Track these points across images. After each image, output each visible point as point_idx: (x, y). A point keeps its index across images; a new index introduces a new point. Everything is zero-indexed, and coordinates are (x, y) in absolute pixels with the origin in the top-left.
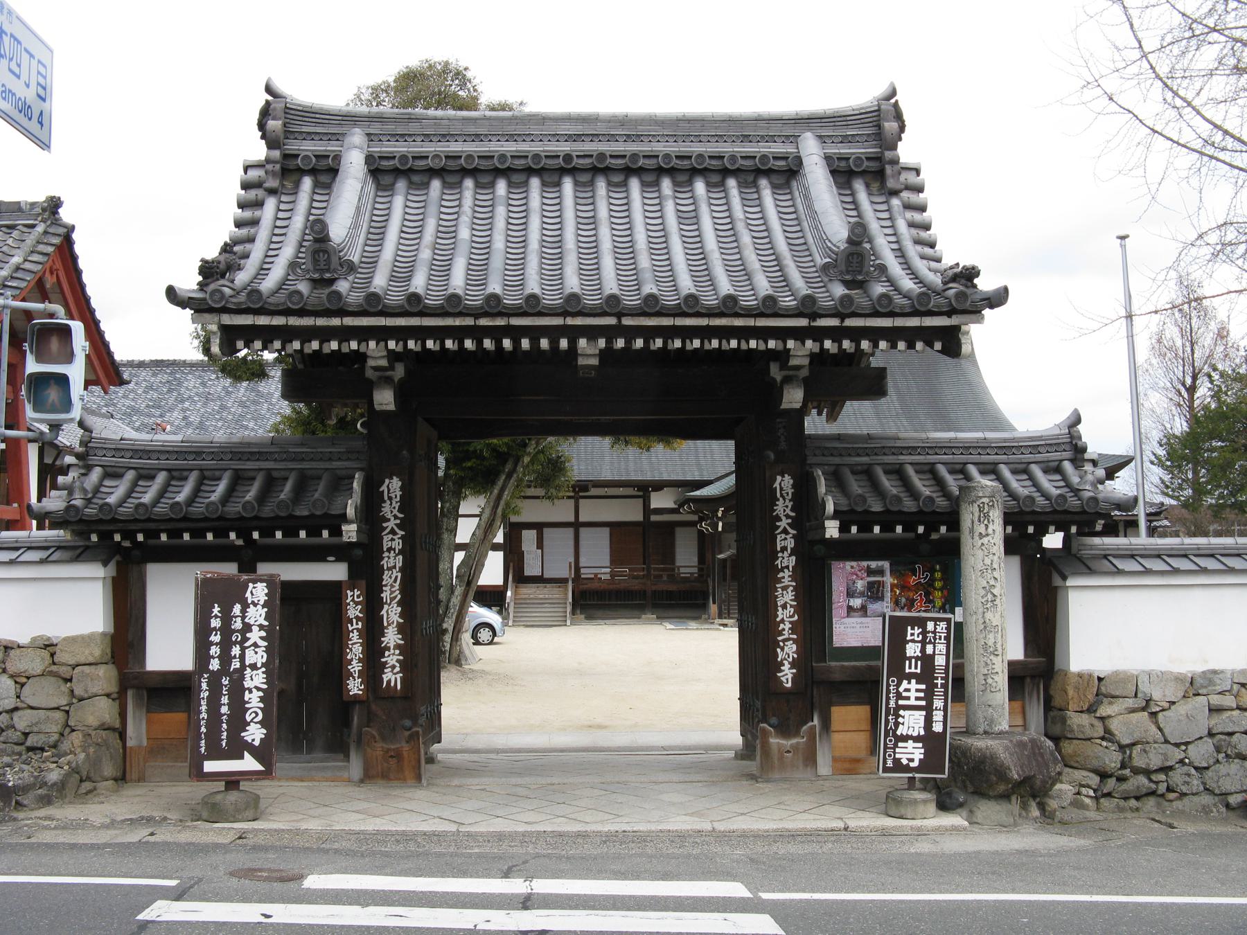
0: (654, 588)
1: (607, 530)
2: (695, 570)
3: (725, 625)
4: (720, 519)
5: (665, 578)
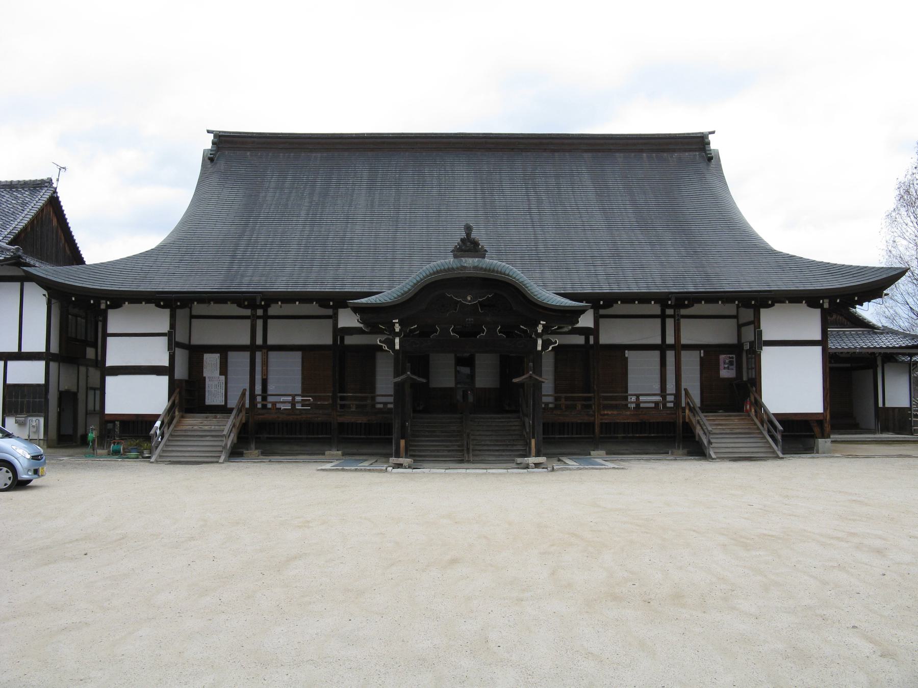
0: (340, 420)
1: (298, 355)
2: (391, 399)
3: (400, 466)
4: (398, 334)
5: (579, 407)
